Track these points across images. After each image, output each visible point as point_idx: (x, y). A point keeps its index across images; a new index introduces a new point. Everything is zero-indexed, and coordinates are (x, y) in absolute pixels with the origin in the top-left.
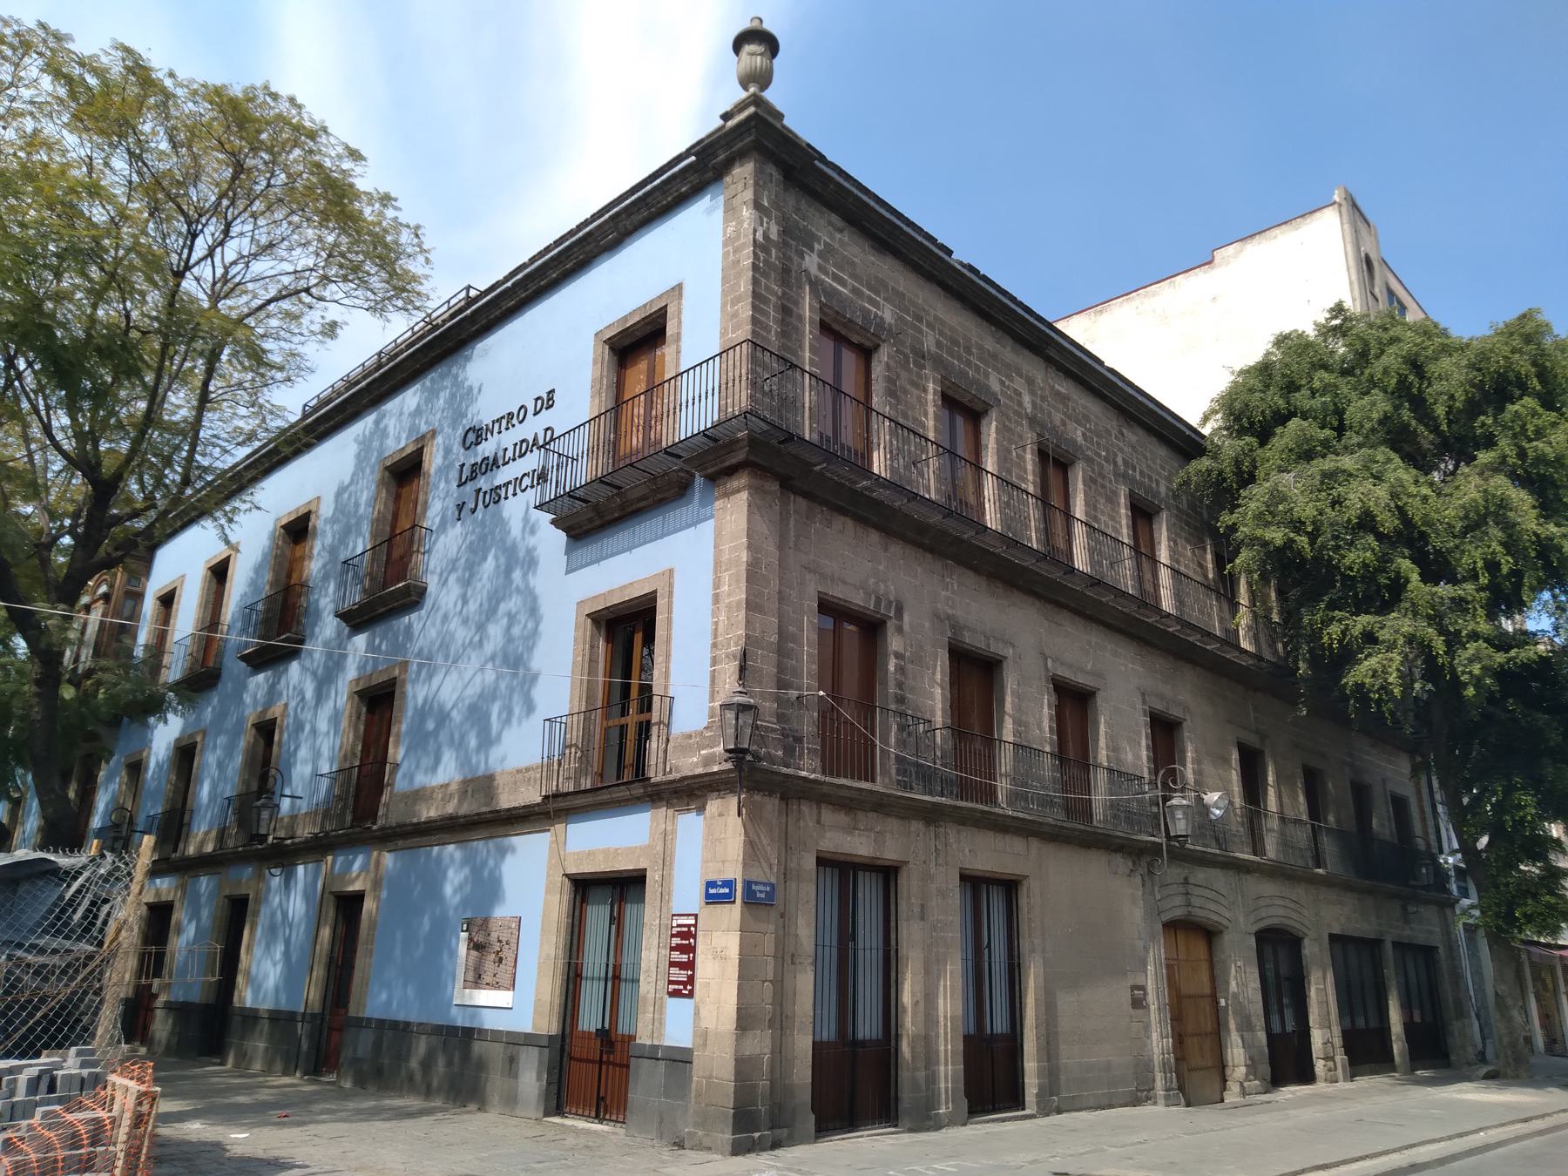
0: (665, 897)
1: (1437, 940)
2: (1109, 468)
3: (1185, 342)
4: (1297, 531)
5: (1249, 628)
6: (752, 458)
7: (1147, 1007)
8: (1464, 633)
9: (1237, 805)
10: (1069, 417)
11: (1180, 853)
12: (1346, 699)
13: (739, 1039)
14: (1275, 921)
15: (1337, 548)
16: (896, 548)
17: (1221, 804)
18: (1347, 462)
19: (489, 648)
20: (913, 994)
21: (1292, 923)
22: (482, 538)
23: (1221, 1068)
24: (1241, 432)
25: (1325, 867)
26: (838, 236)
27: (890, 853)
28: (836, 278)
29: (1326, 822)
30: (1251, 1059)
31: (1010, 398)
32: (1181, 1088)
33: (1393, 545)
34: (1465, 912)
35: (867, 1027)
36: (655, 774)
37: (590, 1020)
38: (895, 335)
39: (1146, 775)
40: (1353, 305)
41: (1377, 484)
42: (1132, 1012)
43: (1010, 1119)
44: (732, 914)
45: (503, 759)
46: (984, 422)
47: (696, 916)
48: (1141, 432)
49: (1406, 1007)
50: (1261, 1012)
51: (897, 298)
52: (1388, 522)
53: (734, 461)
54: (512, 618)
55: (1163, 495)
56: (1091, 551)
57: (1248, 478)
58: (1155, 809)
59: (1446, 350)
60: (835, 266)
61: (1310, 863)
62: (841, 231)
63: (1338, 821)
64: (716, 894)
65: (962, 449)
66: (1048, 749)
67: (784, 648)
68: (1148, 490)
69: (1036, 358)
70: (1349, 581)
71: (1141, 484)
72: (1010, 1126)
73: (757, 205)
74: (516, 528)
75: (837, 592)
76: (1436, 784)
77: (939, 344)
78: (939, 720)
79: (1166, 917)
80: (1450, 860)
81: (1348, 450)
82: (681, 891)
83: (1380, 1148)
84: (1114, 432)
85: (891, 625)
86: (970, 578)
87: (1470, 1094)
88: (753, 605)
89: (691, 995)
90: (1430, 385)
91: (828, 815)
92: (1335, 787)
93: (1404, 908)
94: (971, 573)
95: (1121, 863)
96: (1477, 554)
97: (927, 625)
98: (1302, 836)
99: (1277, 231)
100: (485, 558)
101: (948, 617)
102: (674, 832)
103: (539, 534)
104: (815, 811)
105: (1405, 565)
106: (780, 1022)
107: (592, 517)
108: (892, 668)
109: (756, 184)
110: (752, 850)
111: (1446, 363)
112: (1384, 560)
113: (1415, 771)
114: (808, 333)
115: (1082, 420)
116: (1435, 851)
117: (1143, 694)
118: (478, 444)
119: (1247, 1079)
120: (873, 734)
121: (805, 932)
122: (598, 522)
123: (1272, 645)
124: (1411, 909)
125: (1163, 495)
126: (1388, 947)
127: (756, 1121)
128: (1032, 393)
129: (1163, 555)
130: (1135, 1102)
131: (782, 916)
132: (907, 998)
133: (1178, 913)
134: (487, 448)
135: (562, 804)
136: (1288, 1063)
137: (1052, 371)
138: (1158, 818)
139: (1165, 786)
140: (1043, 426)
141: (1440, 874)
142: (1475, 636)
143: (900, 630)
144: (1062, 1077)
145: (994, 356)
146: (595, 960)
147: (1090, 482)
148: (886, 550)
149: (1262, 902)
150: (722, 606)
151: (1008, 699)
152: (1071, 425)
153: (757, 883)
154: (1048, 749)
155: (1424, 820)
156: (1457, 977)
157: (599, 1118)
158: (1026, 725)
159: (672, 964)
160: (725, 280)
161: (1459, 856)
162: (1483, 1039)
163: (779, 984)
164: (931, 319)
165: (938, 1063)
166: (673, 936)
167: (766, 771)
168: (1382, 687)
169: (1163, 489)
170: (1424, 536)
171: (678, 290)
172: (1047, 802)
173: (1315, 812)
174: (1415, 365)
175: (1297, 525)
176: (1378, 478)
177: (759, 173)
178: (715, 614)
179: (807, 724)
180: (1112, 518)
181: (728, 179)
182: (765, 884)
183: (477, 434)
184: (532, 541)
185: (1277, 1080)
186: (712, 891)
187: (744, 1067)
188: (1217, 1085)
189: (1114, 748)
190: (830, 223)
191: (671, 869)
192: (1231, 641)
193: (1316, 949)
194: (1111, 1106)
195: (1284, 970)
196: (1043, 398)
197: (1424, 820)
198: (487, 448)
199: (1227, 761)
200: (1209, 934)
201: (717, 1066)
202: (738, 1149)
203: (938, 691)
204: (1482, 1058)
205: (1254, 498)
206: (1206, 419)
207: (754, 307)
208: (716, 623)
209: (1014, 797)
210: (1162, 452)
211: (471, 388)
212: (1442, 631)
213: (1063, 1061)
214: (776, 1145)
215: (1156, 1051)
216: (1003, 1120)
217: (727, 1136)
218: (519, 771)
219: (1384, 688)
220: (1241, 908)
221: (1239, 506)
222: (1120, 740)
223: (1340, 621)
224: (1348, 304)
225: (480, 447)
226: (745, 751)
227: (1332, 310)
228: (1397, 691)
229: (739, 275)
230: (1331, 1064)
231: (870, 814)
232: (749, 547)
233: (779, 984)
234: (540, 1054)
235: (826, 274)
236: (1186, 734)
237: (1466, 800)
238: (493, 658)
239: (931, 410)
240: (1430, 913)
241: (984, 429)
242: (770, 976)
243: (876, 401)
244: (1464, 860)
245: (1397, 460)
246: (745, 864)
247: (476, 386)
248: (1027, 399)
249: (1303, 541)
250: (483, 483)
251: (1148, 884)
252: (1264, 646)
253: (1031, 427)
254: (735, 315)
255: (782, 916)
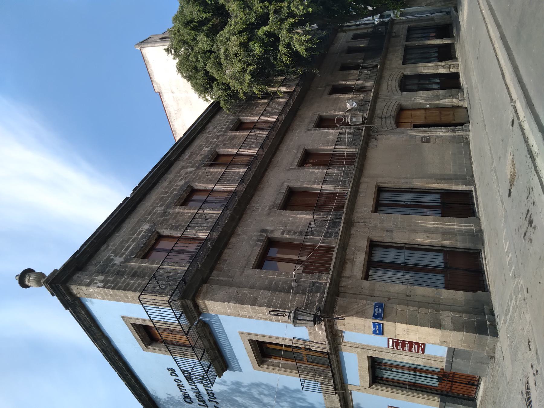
0: (380, 350)
1: (406, 26)
2: (221, 138)
3: (185, 105)
4: (246, 70)
5: (287, 88)
6: (190, 298)
7: (430, 136)
8: (288, 11)
9: (353, 96)
10: (199, 153)
11: (370, 120)
12: (312, 56)
13: (445, 328)
14: (397, 84)
15: (254, 56)
16: (239, 230)
17: (351, 103)
18: (222, 50)
19: (273, 403)
20: (424, 238)
21: (398, 78)
22: (228, 401)
23: (454, 108)
24: (211, 87)
25: (378, 65)
26: (110, 247)
27: (364, 244)
28: (126, 250)
29: (360, 63)
30: (450, 96)
31: (188, 177)
32: (462, 124)
33: (254, 35)
34: (396, 16)
35: (438, 260)
36: (327, 348)
37: (435, 383)
38: (154, 224)
39: (340, 131)
40: (166, 45)
41: (229, 40)
42: (432, 142)
43: (477, 198)
44: (388, 325)
45: (320, 403)
46: (196, 188)
47: (389, 339)
48: (209, 125)
49: (429, 38)
50: (432, 91)
51: (140, 223)
52: (244, 37)
53: (192, 305)
54: (261, 393)
55: (234, 117)
56: (251, 147)
57: (227, 87)
58: (352, 128)
59: (181, 12)
60: (121, 249)
61: (376, 70)
62: (108, 245)
63: (361, 59)
64: (379, 331)
65: (203, 197)
66: (325, 170)
67: (273, 288)
68: (231, 123)
69: (174, 165)
70: (266, 52)
71: (228, 126)
72: (480, 199)
73: (88, 285)
74: (224, 388)
75: (253, 259)
76: (348, 24)
77: (161, 206)
78: (310, 217)
79: (394, 127)
80: (377, 20)
81: (219, 50)
82: (379, 344)
83: (492, 51)
84: (208, 135)
85: (270, 235)
86: (255, 199)
87: (464, 16)
88: (254, 303)
89: (424, 345)
90: (194, 19)
91: (347, 273)
92: (349, 60)
93: (394, 37)
94: (253, 198)
95: (373, 143)
96: (257, 5)
97: (272, 219)
98: (366, 72)
99: (149, 69)
100: (237, 401)
101: (270, 209)
102: (351, 343)
103: (226, 380)
104: (345, 279)
105: (260, 32)
106: (436, 305)
107: (218, 359)
108: (288, 236)
109: (80, 285)
110: (360, 313)
111: (186, 12)
112: (259, 39)
113: (344, 31)
114: (146, 264)
115: (201, 147)
116: (373, 25)
117: (308, 130)
118: (190, 398)
119: (458, 98)
120: (315, 246)
121: (398, 288)
122: (220, 359)
123: (294, 80)
124: (394, 34)
125: (234, 117)
126: (408, 43)
127: (482, 322)
128: (187, 167)
129: (255, 119)
130: (468, 144)
131: (389, 299)
132: (426, 241)
133: (393, 121)
134: (192, 395)
135: (339, 387)
136: (451, 82)
137: (181, 159)
138: (357, 127)
139: (343, 124)
140: (201, 164)
141: (381, 24)
142: (289, 8)
143: (272, 231)
144: (459, 173)
145: (171, 182)
146: (408, 378)
147: (225, 146)
148: (239, 235)
149: (390, 89)
150: (254, 315)
151: (305, 185)
152: (202, 152)
153: (375, 312)
154: (325, 170)
155: (362, 29)
156: (419, 20)
157: (477, 385)
158: (316, 179)
159: (410, 350)
160: (119, 300)
161: (375, 17)
162: (441, 12)
163: (421, 304)
164: (151, 208)
165: (454, 229)
166: (397, 349)
167: (325, 304)
168: (307, 42)
169: (232, 118)
170: (251, 24)
171: (124, 318)
172: (346, 174)
173: (356, 68)
174: (187, 23)
175: (244, 70)
176: (228, 39)
177: (76, 283)
178: (257, 318)
179: (307, 279)
180: (240, 138)
181: (78, 296)
182: (375, 308)
183: (186, 397)
184: (229, 383)
185: (458, 87)
186: (378, 332)
187: (457, 327)
188: (460, 110)
189: (328, 143)
190: (104, 250)
191: (368, 346)
192: (290, 95)
193: (408, 69)
194: (470, 154)
195: (416, 82)
196: (190, 163)
197: (362, 29)
198: (192, 395)
199: (336, 99)
200: (401, 110)
201: (458, 339)
202: (495, 334)
203: (299, 216)
204: (448, 13)
205: (234, 85)
206: (207, 100)
207: (129, 290)
208: (261, 318)
209: (344, 185)
210: (218, 117)
211: (168, 398)
212: (286, 19)
213: (452, 173)
214: (492, 313)
215: (447, 134)
216: (477, 201)
217: (489, 339)
218: (325, 399)
219: (307, 41)
220: (392, 97)
221: (237, 90)
222: (324, 141)
223: (281, 56)
224: (166, 47)
225: (192, 397)
226: (315, 317)
227: (168, 53)
228: (308, 37)
229: (116, 295)
230: (452, 66)
231: (347, 252)
232: (229, 302)
233: (421, 304)
234: (448, 406)
235: (124, 253)
236: (324, 114)
237: (354, 13)
238: (277, 402)
239: (186, 211)
240: (396, 28)
241: (198, 188)
242: (416, 309)
243: (179, 235)
244: (376, 15)
245: (221, 33)
246: (366, 317)
247: (167, 396)
248: (189, 170)
249: (250, 68)
250: (206, 398)
251: (381, 133)
252: (294, 83)
253: (200, 169)
254: (133, 298)
255: (389, 299)
